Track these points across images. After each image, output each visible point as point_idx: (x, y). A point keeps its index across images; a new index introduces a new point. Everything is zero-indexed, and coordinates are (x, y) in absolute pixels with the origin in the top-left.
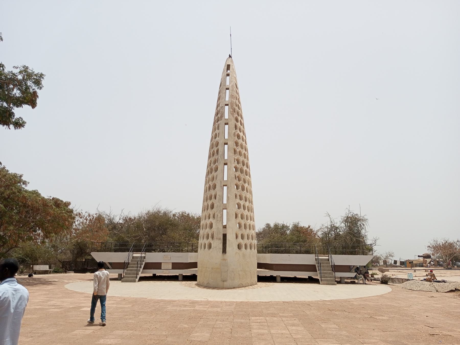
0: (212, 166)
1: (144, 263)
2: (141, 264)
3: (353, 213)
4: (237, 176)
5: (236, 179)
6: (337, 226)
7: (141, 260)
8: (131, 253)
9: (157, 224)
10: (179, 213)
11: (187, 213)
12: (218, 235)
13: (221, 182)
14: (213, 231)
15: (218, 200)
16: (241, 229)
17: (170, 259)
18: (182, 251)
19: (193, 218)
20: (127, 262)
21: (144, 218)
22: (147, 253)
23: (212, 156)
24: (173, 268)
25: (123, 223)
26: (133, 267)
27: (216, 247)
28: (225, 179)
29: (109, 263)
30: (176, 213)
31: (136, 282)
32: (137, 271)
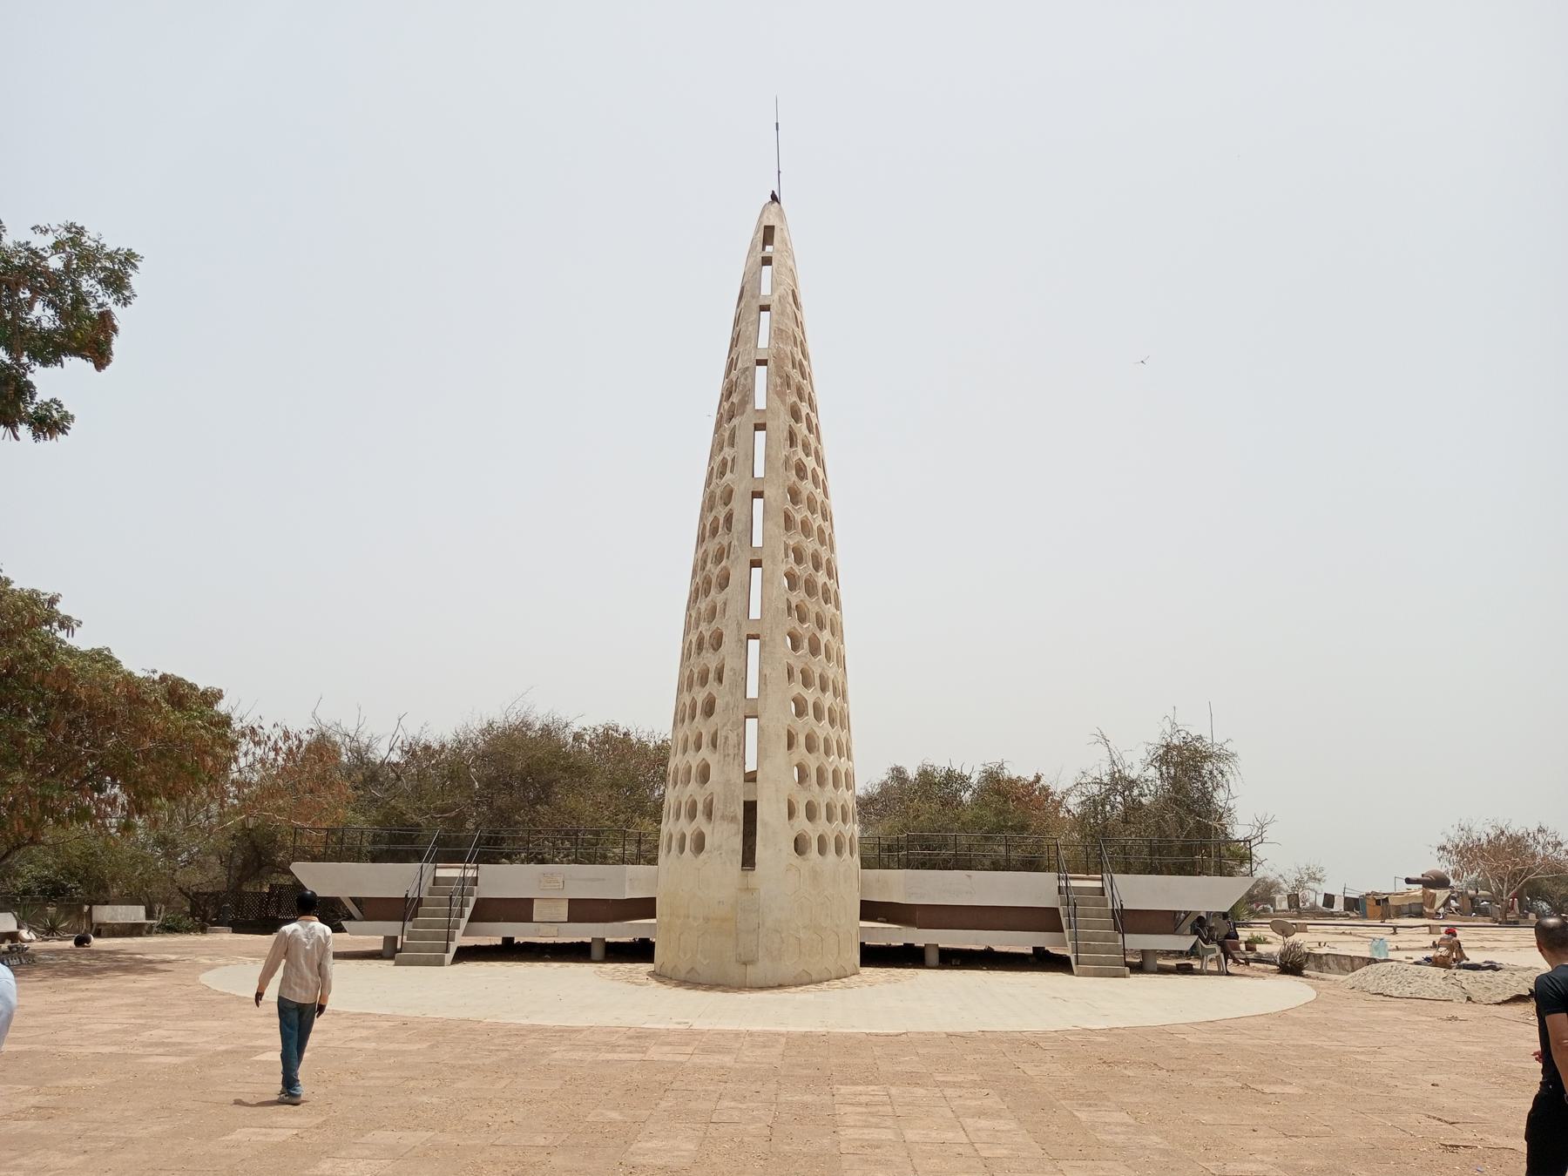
0: (710, 571)
1: (472, 901)
2: (463, 904)
3: (1188, 734)
4: (793, 606)
5: (789, 614)
7: (463, 889)
8: (429, 866)
9: (519, 766)
11: (622, 730)
13: (739, 625)
15: (728, 687)
17: (561, 887)
19: (643, 746)
20: (416, 896)
21: (475, 745)
22: (485, 868)
24: (572, 918)
25: (402, 762)
26: (434, 914)
28: (755, 613)
29: (353, 900)
30: (585, 729)
31: (443, 965)
32: (449, 928)
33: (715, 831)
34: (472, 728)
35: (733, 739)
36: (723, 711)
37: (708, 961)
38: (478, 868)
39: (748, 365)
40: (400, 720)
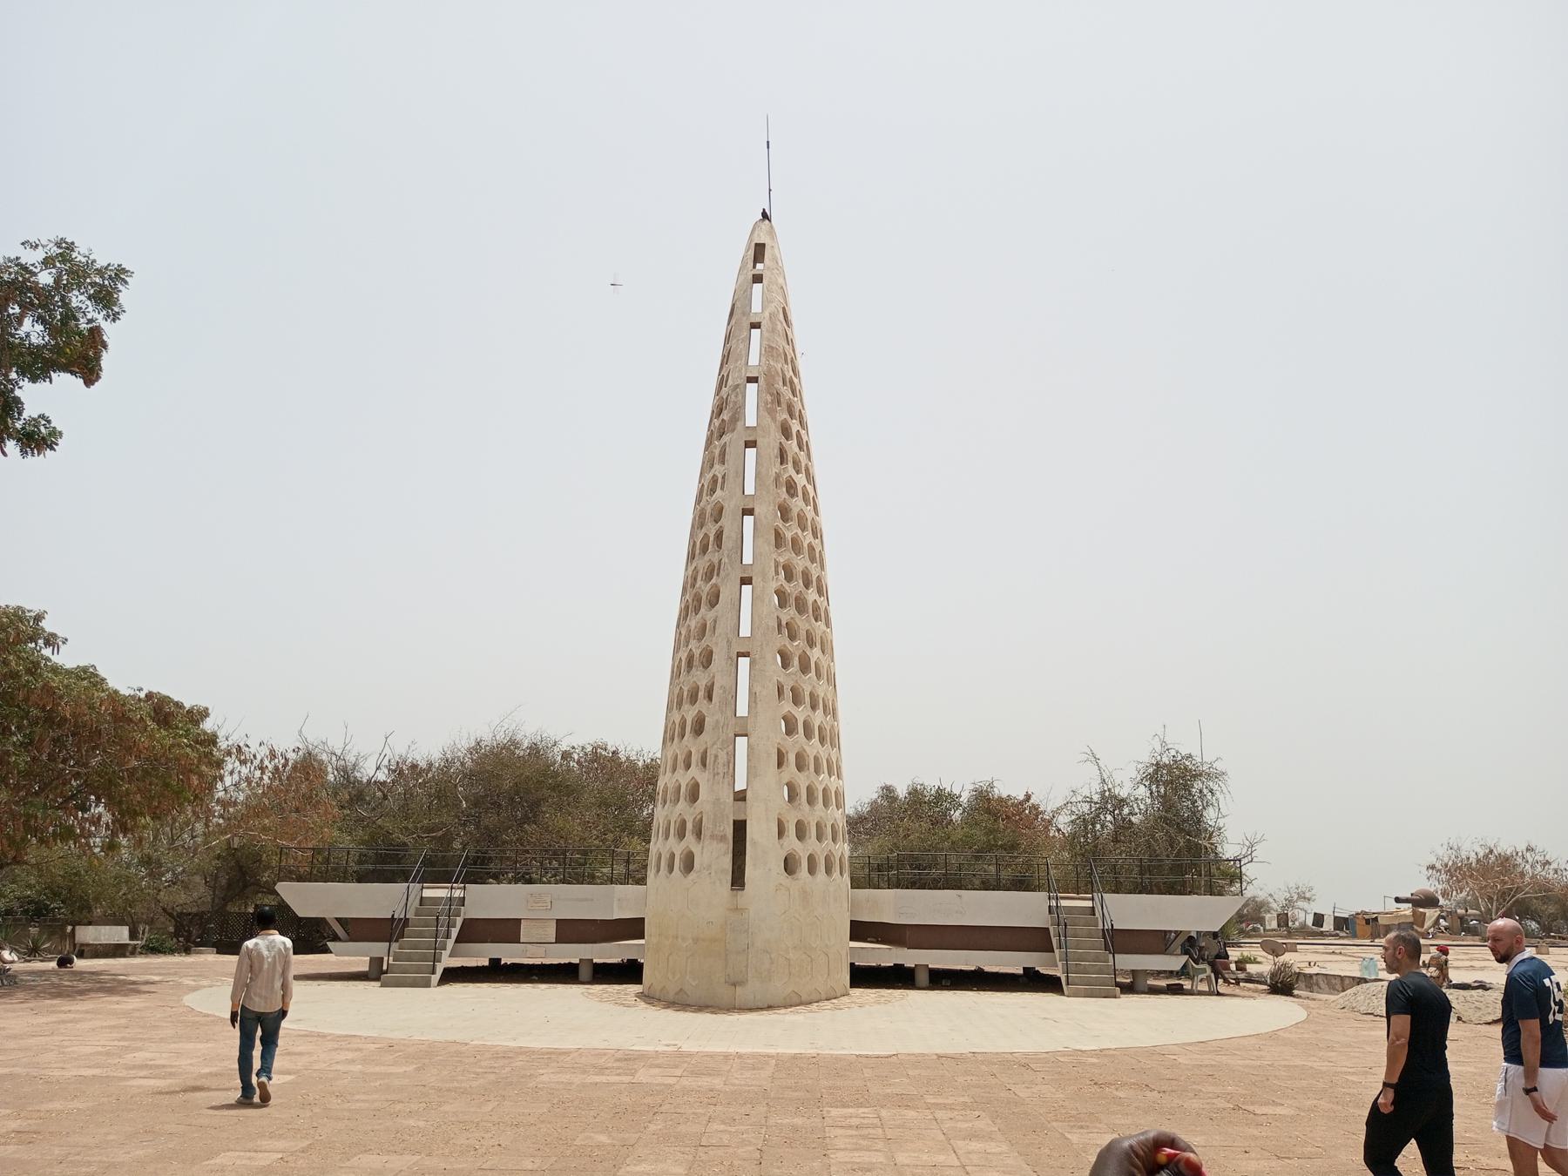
0: (700, 588)
1: (459, 921)
2: (450, 925)
4: (784, 623)
5: (780, 632)
6: (1123, 793)
10: (583, 748)
11: (611, 749)
12: (716, 825)
14: (701, 812)
16: (796, 803)
18: (592, 880)
19: (632, 764)
20: (402, 916)
21: (462, 764)
23: (699, 554)
24: (560, 939)
26: (420, 934)
27: (709, 866)
29: (338, 920)
31: (430, 987)
32: (435, 949)
33: (705, 850)
34: (460, 746)
35: (723, 757)
36: (713, 729)
37: (697, 982)
38: (465, 887)
39: (739, 382)
40: (386, 738)
